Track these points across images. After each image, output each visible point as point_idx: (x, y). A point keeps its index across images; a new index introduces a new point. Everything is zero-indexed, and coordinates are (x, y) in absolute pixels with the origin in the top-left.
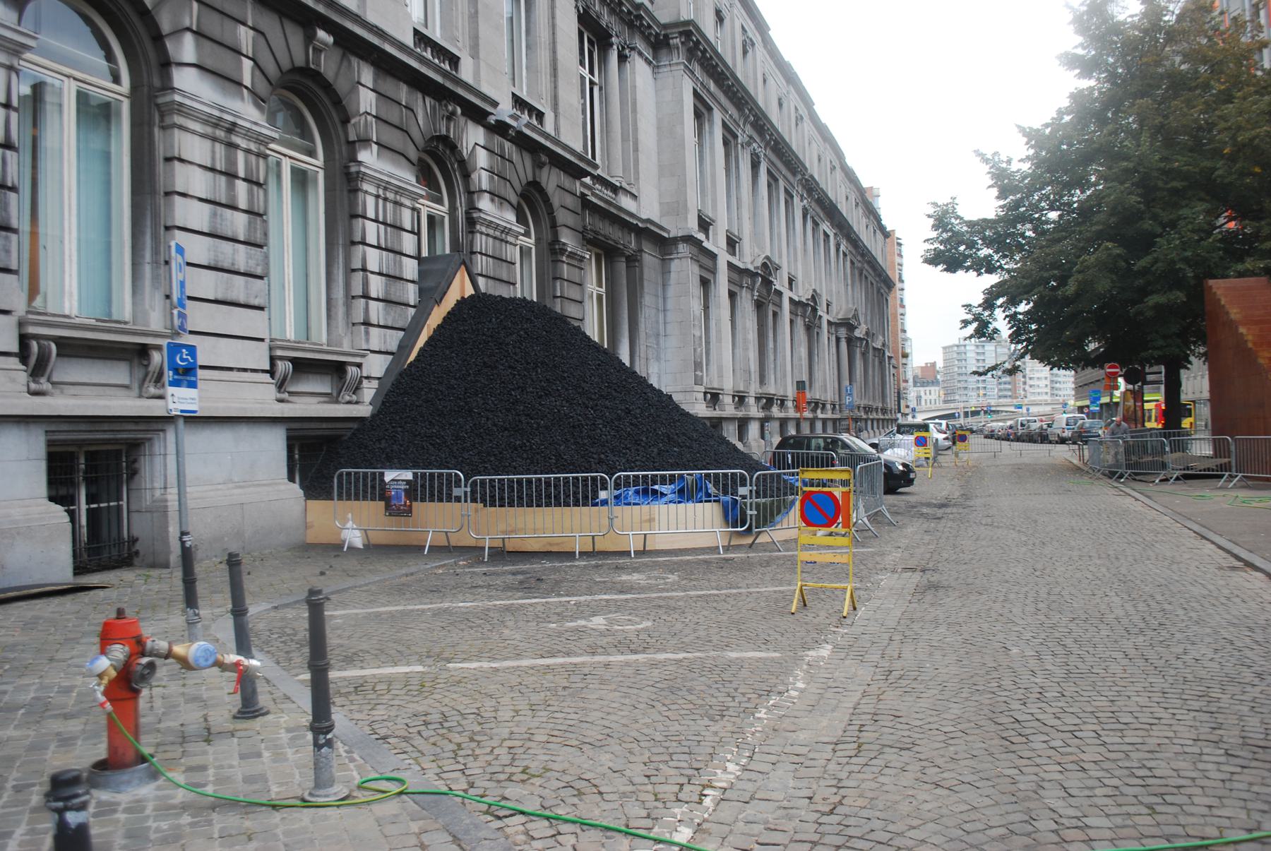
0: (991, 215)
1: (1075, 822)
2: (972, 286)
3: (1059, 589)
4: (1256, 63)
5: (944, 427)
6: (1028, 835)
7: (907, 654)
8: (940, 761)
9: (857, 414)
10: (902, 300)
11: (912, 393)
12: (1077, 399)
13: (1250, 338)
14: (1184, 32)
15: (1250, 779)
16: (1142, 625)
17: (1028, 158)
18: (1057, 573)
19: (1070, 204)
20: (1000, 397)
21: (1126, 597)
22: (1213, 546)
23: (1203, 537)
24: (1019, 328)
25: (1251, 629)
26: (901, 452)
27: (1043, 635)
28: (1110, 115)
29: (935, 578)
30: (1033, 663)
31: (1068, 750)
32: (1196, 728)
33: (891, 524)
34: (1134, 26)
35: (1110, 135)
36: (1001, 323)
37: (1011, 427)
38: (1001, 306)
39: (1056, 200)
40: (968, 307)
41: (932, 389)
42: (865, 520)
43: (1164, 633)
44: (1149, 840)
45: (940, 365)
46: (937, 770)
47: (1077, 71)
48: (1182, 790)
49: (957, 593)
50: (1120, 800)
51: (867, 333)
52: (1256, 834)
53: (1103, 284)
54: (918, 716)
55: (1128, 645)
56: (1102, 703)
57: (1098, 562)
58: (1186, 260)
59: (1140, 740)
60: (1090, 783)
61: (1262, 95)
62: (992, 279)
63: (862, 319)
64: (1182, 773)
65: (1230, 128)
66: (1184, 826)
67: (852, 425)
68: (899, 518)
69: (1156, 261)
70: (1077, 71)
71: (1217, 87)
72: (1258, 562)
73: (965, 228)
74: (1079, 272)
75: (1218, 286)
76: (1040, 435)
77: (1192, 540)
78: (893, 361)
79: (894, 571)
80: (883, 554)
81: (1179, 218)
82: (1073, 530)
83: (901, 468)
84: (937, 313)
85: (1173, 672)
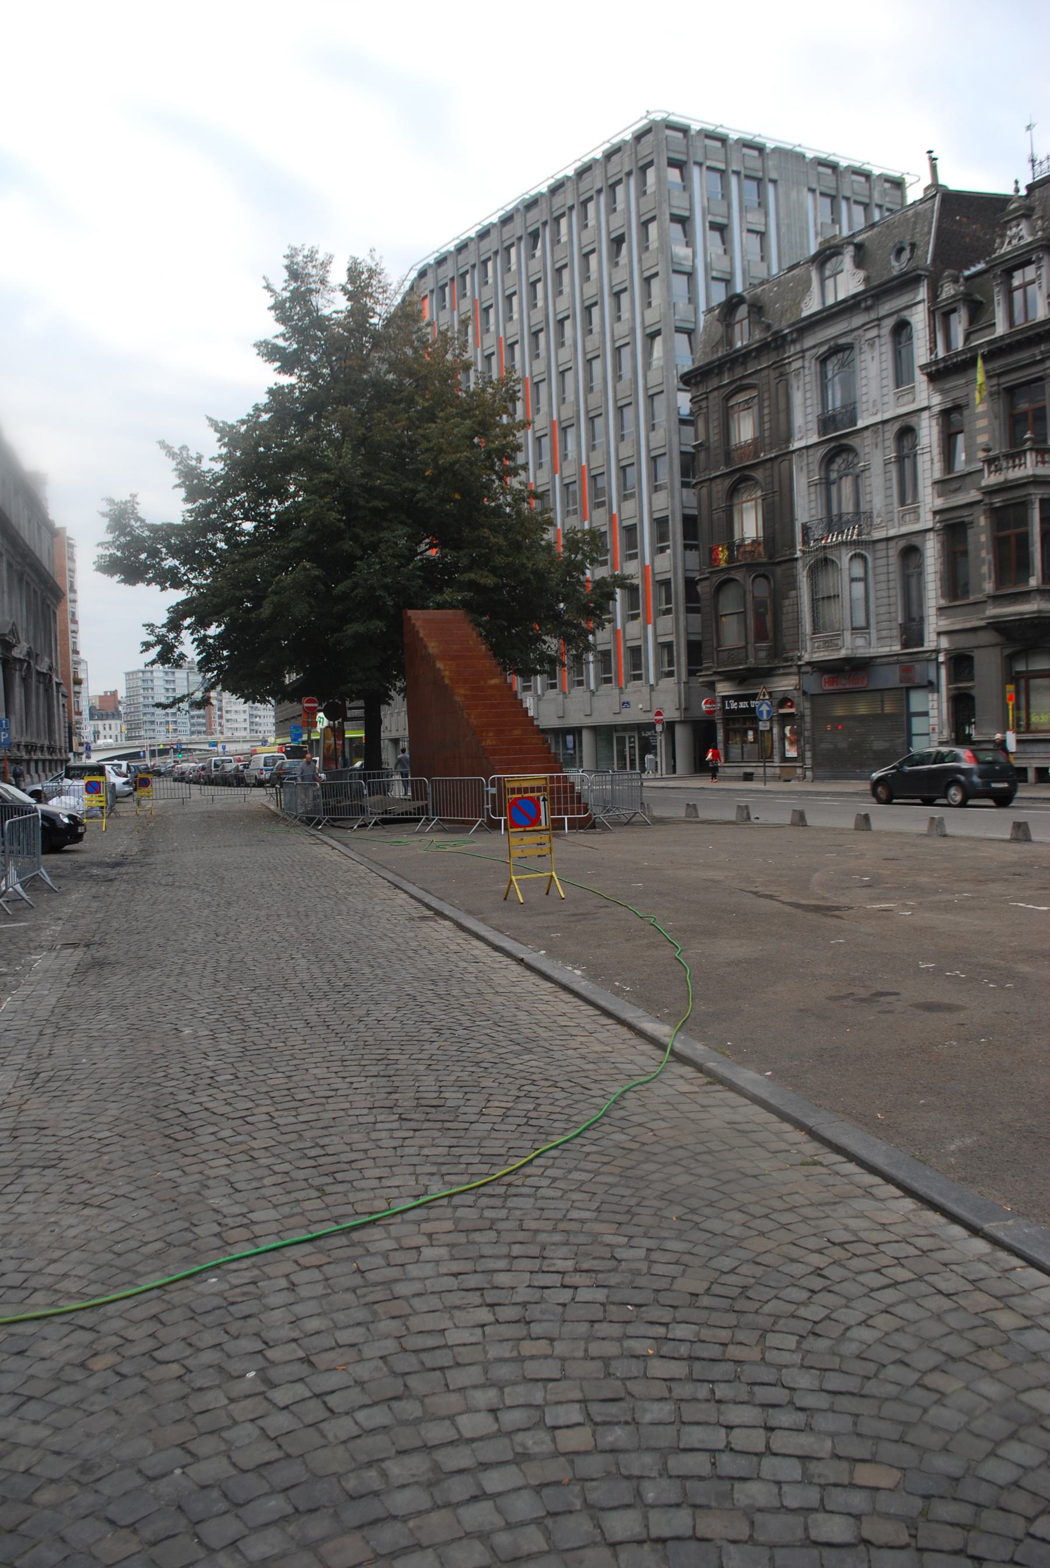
0: (178, 520)
1: (240, 1220)
2: (157, 602)
3: (242, 955)
4: (460, 383)
5: (124, 769)
6: (188, 1244)
7: (60, 1049)
8: (90, 1175)
9: (16, 753)
10: (73, 614)
11: (87, 728)
12: (278, 736)
13: (447, 673)
14: (389, 338)
15: (422, 1142)
16: (327, 988)
17: (221, 457)
18: (241, 937)
19: (267, 515)
20: (192, 733)
21: (313, 958)
22: (405, 896)
23: (397, 887)
24: (209, 655)
25: (434, 982)
26: (68, 802)
27: (220, 1011)
28: (312, 418)
29: (100, 953)
30: (206, 1043)
31: (239, 1138)
32: (372, 1095)
33: (51, 890)
34: (339, 324)
35: (311, 441)
36: (188, 648)
37: (203, 768)
38: (188, 628)
39: (253, 509)
40: (150, 626)
41: (113, 722)
42: (18, 887)
43: (348, 995)
44: (317, 1226)
45: (122, 694)
46: (86, 1186)
47: (278, 364)
48: (354, 1165)
49: (125, 970)
50: (290, 1186)
51: (29, 654)
52: (422, 1200)
53: (300, 608)
54: (68, 1124)
55: (310, 1012)
56: (278, 1079)
57: (287, 921)
58: (385, 587)
59: (314, 1117)
60: (259, 1173)
61: (464, 419)
62: (179, 595)
63: (22, 636)
64: (355, 1147)
65: (432, 449)
66: (353, 1204)
67: (10, 768)
68: (62, 882)
69: (356, 586)
70: (278, 364)
71: (421, 404)
72: (448, 910)
73: (147, 533)
74: (275, 593)
75: (416, 616)
76: (236, 777)
77: (385, 891)
78: (63, 689)
79: (51, 949)
80: (38, 929)
81: (380, 541)
82: (262, 886)
83: (66, 820)
84: (116, 633)
85: (353, 1037)
